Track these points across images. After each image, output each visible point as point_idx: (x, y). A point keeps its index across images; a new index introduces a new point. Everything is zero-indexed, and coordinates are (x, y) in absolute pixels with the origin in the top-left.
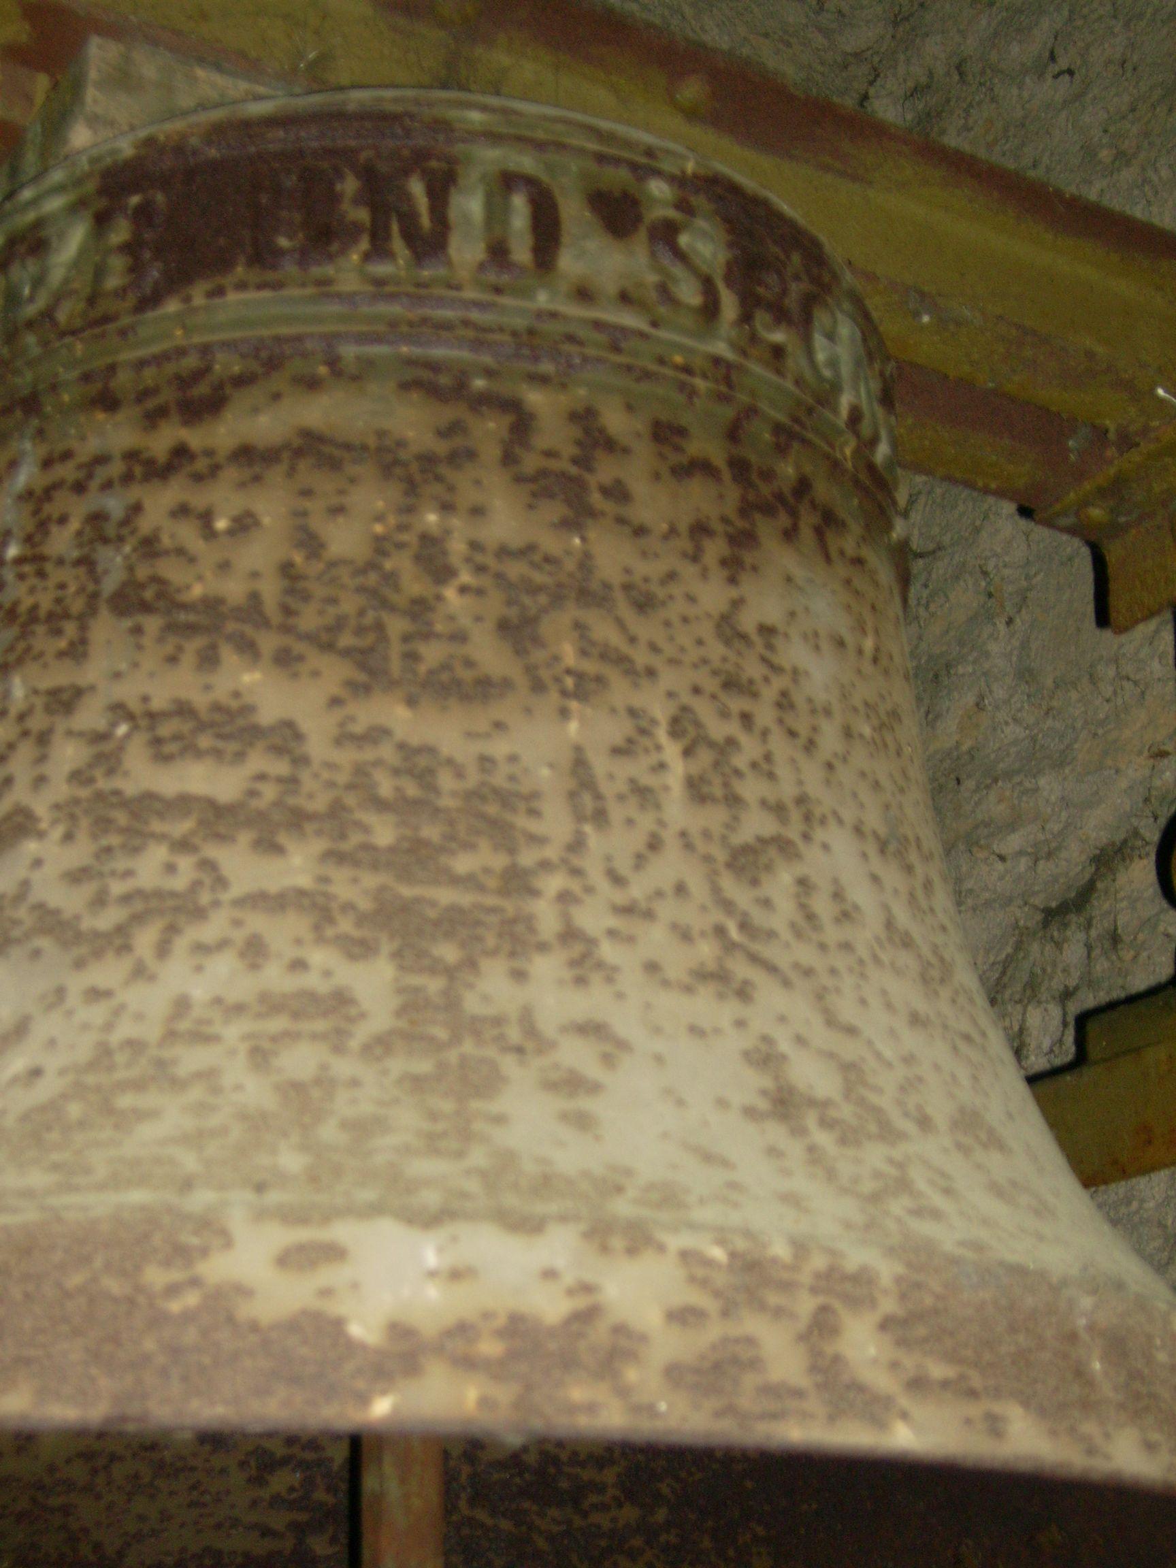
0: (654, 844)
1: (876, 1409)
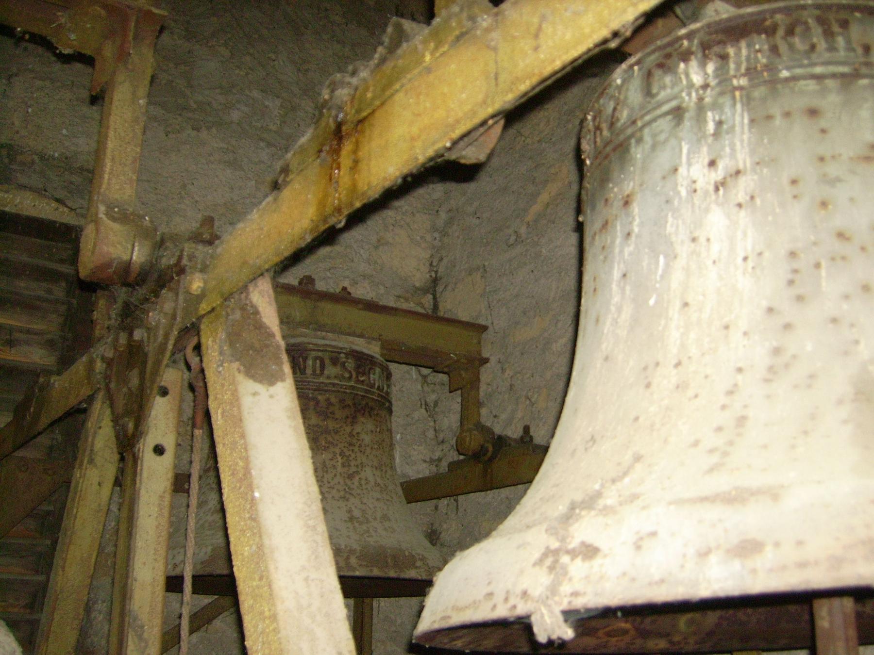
0: (335, 475)
1: (354, 569)
